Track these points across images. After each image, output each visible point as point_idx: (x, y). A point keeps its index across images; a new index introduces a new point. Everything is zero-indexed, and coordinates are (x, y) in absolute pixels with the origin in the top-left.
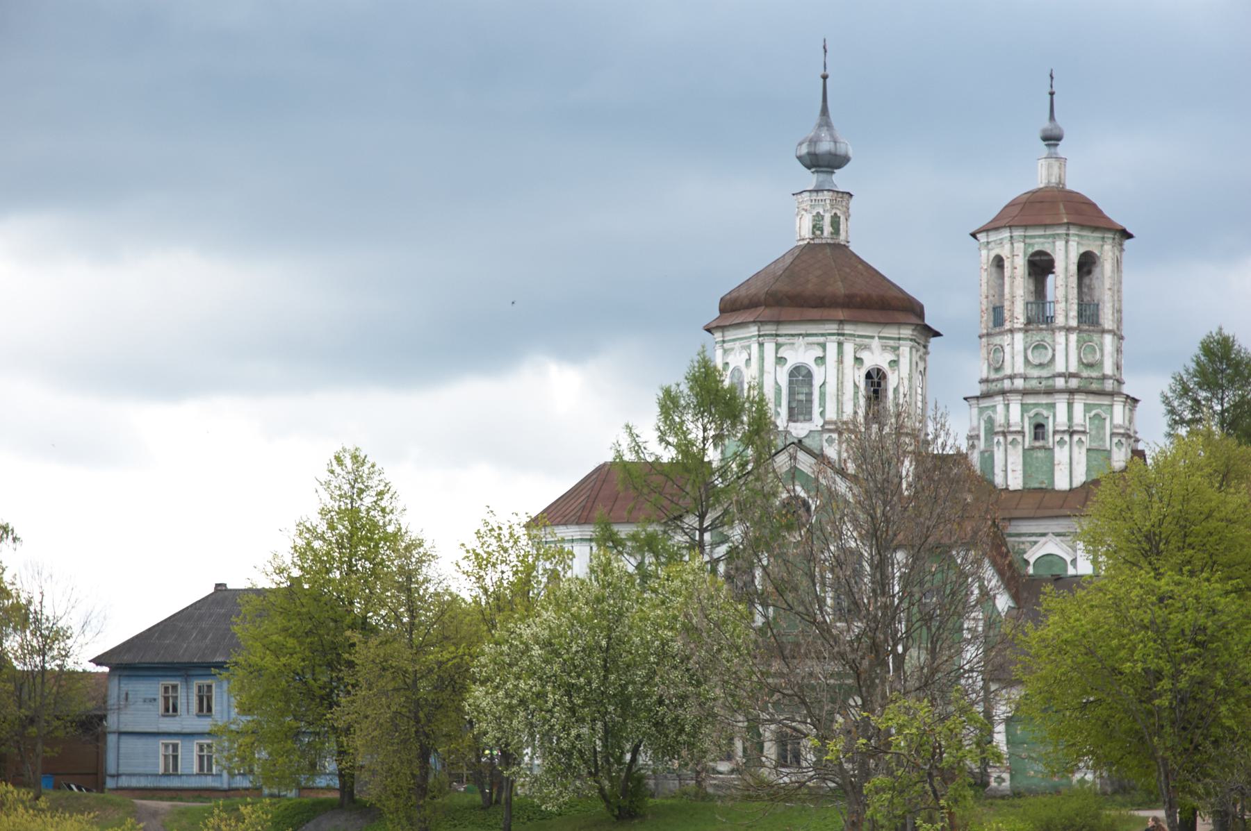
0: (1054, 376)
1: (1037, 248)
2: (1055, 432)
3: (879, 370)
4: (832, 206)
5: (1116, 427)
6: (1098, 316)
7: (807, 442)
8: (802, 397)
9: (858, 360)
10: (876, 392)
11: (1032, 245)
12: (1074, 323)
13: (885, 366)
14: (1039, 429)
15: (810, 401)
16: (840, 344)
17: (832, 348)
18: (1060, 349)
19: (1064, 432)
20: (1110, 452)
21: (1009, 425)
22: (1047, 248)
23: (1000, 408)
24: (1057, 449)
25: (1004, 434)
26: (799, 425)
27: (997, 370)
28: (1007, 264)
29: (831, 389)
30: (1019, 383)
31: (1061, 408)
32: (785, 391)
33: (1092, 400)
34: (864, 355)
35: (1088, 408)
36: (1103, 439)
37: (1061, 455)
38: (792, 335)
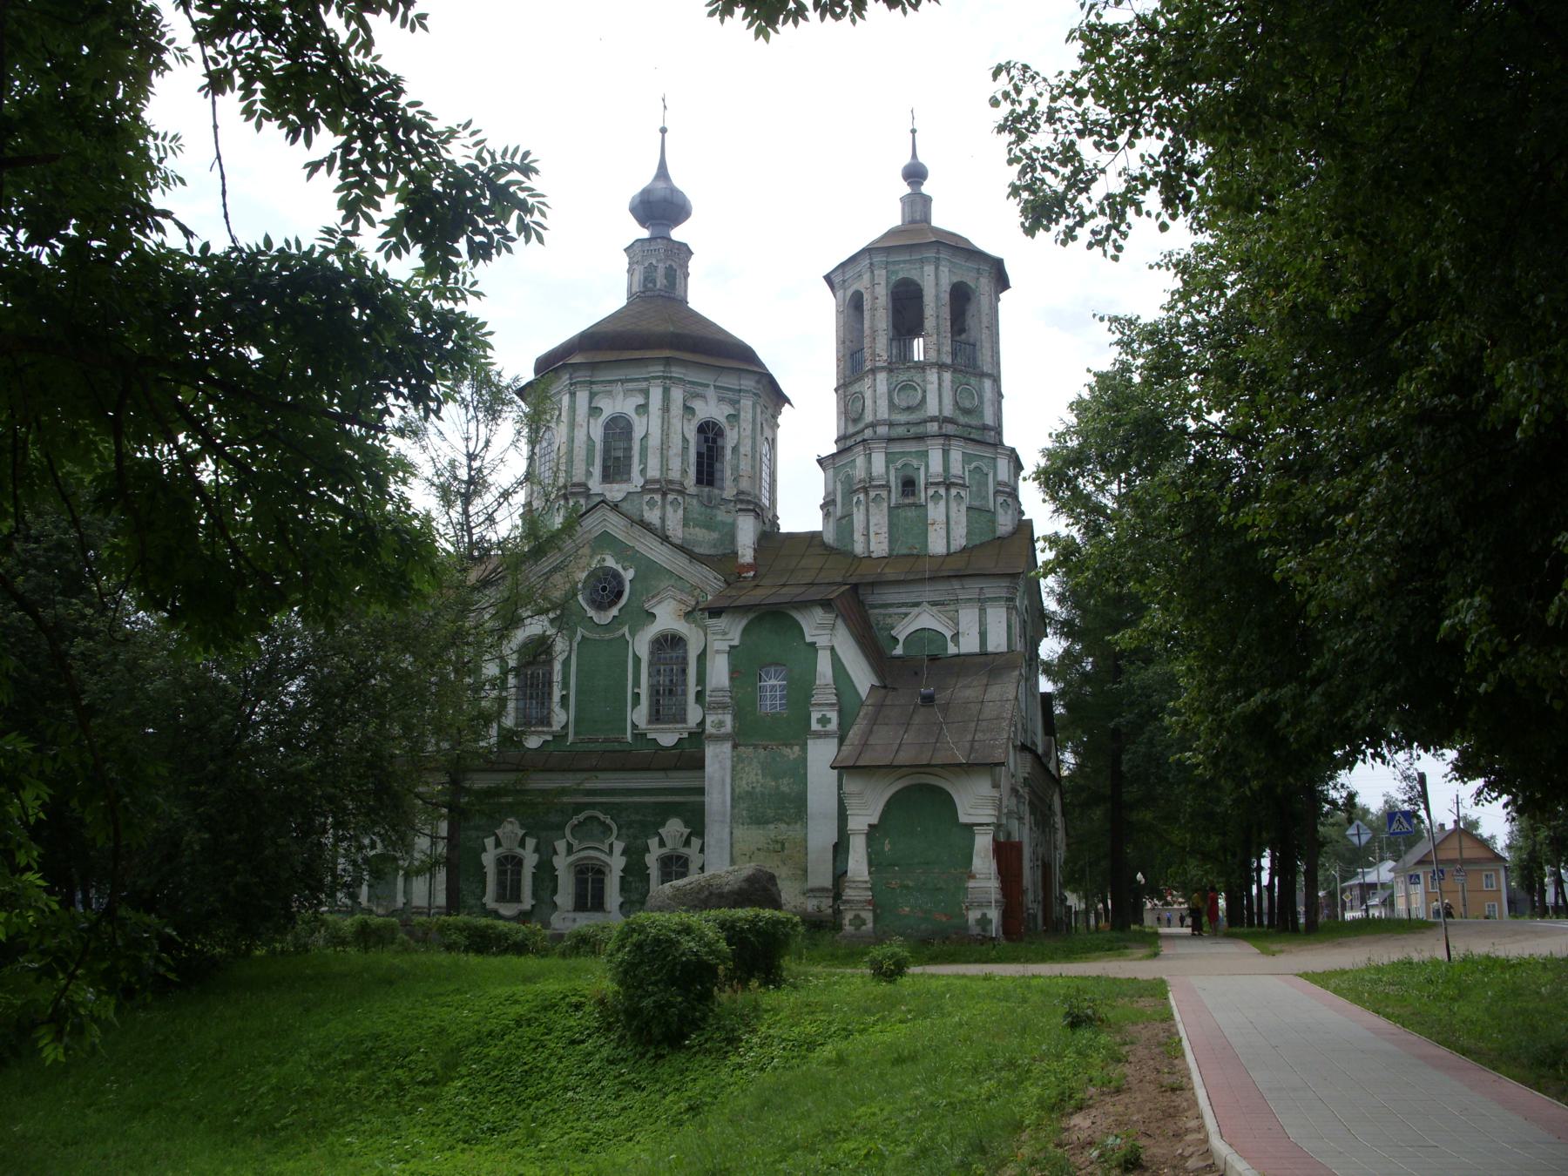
0: (925, 421)
1: (901, 275)
3: (715, 424)
4: (667, 257)
5: (999, 484)
6: (975, 359)
7: (625, 506)
8: (620, 454)
9: (688, 410)
10: (710, 449)
11: (896, 272)
12: (948, 360)
14: (909, 485)
15: (629, 458)
16: (666, 391)
17: (656, 395)
18: (932, 388)
19: (937, 484)
20: (994, 513)
21: (871, 479)
22: (914, 275)
23: (860, 461)
24: (930, 506)
25: (866, 490)
26: (616, 486)
27: (855, 421)
28: (867, 306)
29: (654, 441)
30: (882, 430)
31: (935, 458)
32: (599, 446)
33: (972, 449)
34: (697, 405)
35: (967, 458)
36: (986, 498)
37: (936, 512)
38: (610, 382)
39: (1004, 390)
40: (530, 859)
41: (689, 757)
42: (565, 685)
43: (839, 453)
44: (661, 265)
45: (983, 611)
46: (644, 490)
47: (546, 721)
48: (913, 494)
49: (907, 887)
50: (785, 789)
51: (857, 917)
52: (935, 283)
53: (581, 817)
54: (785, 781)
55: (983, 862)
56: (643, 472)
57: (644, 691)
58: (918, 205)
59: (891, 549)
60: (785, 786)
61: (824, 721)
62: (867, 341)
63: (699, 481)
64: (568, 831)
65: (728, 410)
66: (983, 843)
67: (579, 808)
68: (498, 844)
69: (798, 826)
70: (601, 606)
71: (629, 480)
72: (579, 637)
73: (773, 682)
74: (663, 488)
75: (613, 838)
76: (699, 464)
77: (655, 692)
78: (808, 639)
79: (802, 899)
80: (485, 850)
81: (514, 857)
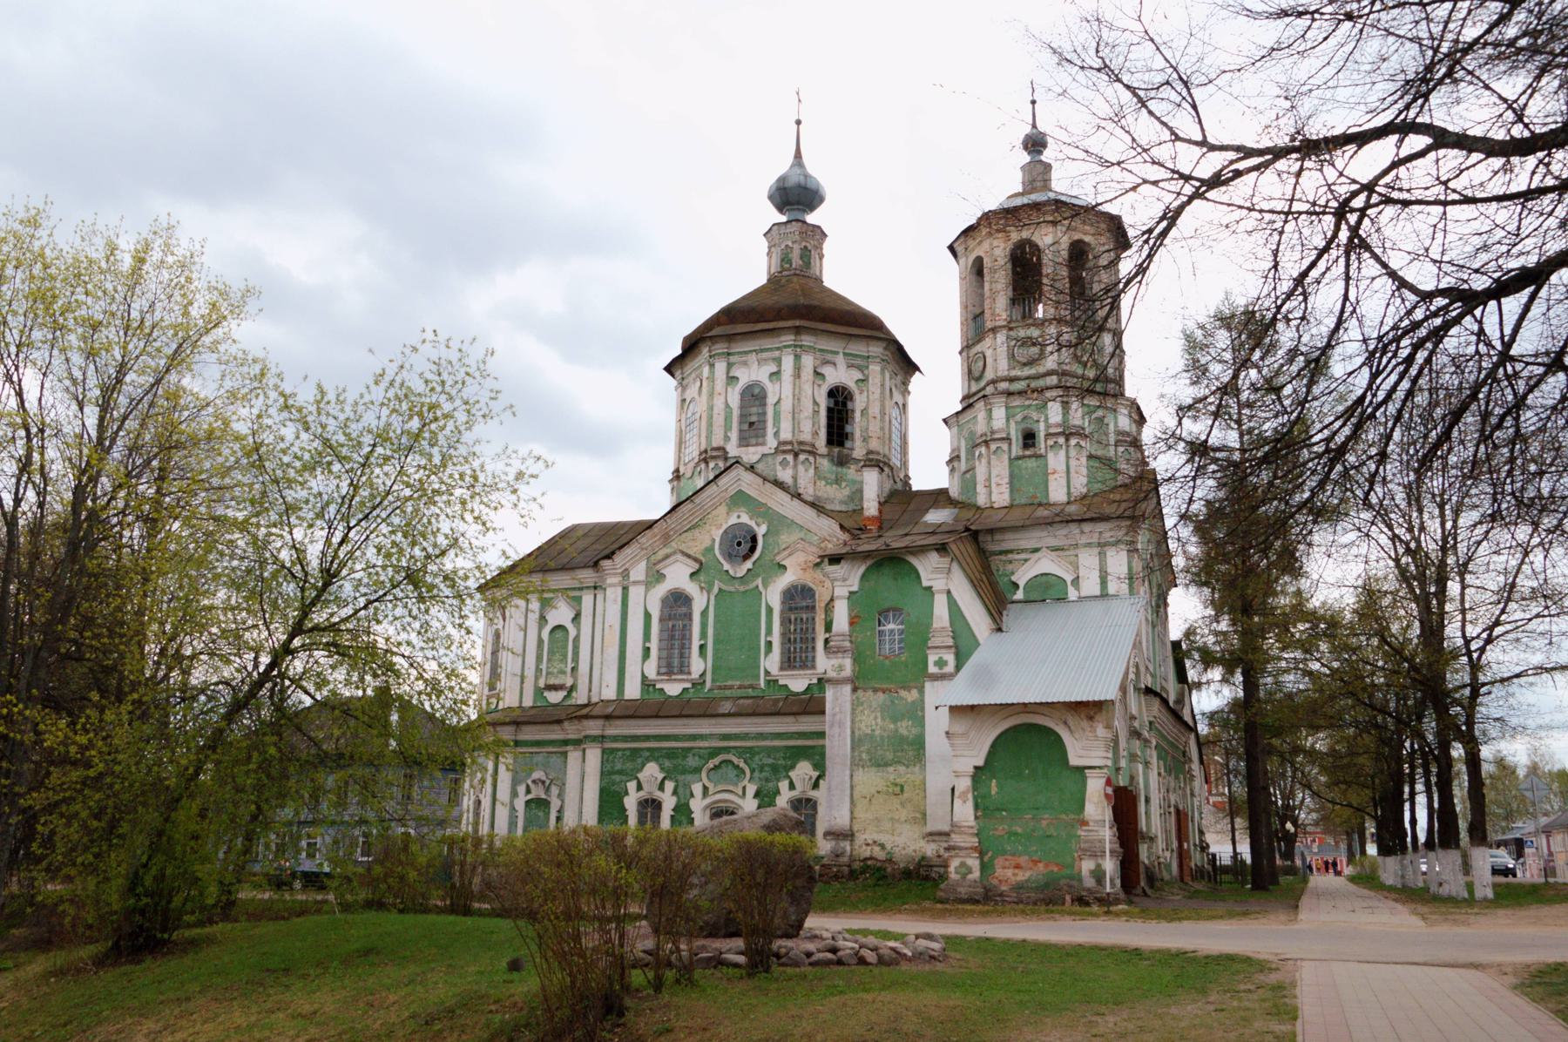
2: (1048, 435)
3: (844, 389)
13: (851, 385)
14: (1029, 438)
16: (797, 357)
17: (788, 362)
24: (1051, 456)
26: (751, 449)
29: (787, 405)
30: (1003, 386)
37: (1056, 461)
39: (1125, 346)
40: (669, 803)
41: (811, 704)
42: (703, 635)
43: (964, 409)
44: (796, 246)
45: (1102, 555)
47: (684, 668)
48: (1033, 445)
49: (1016, 834)
50: (905, 732)
51: (963, 864)
52: (1051, 240)
53: (716, 761)
54: (904, 723)
55: (1097, 808)
56: (776, 434)
57: (776, 639)
58: (1038, 174)
59: (1012, 499)
60: (905, 728)
61: (941, 663)
62: (987, 304)
63: (830, 442)
64: (704, 774)
65: (858, 375)
66: (1095, 787)
67: (715, 752)
68: (639, 787)
69: (917, 769)
72: (716, 590)
73: (891, 626)
74: (796, 450)
75: (746, 782)
76: (830, 426)
77: (786, 639)
78: (925, 583)
79: (922, 843)
80: (627, 793)
81: (654, 801)
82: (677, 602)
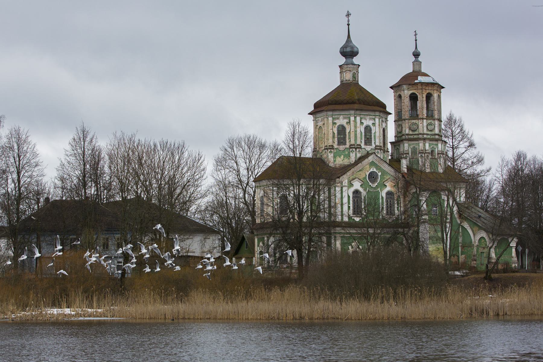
9: (362, 123)
15: (371, 138)
16: (355, 117)
21: (426, 150)
22: (430, 91)
26: (368, 147)
31: (421, 145)
32: (363, 134)
35: (409, 145)
46: (376, 149)
56: (375, 143)
70: (373, 182)
71: (371, 145)
82: (356, 192)
